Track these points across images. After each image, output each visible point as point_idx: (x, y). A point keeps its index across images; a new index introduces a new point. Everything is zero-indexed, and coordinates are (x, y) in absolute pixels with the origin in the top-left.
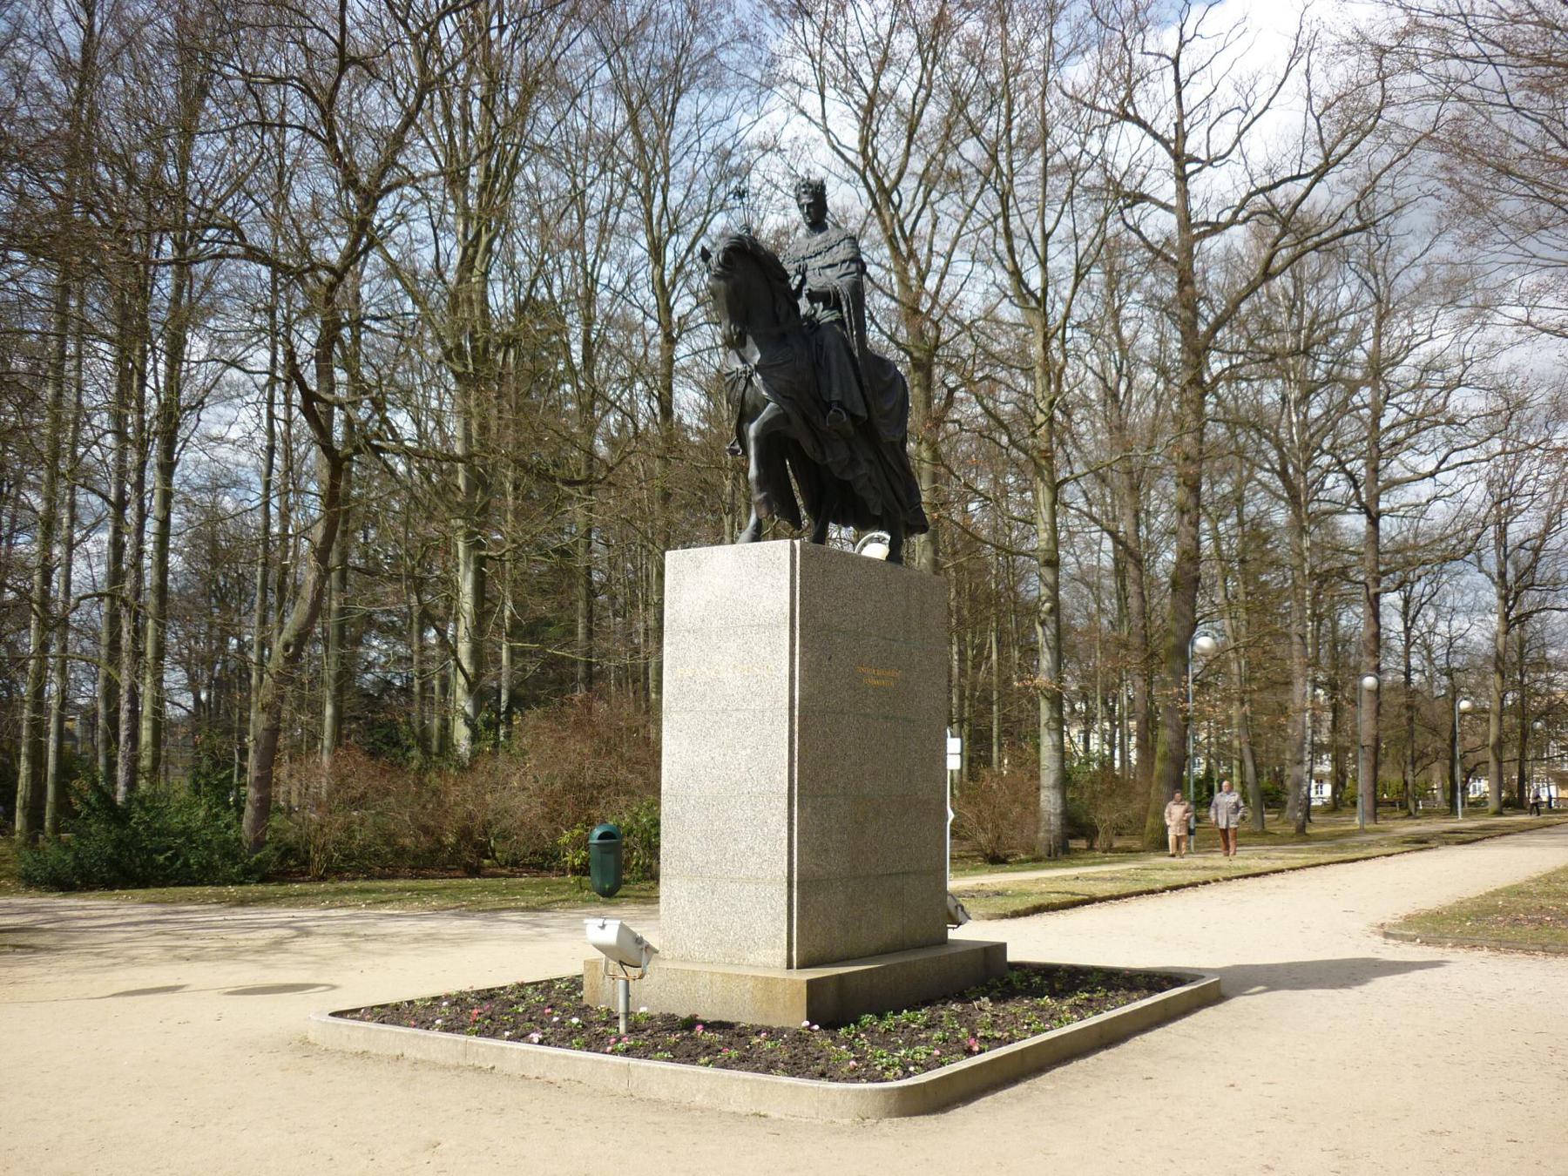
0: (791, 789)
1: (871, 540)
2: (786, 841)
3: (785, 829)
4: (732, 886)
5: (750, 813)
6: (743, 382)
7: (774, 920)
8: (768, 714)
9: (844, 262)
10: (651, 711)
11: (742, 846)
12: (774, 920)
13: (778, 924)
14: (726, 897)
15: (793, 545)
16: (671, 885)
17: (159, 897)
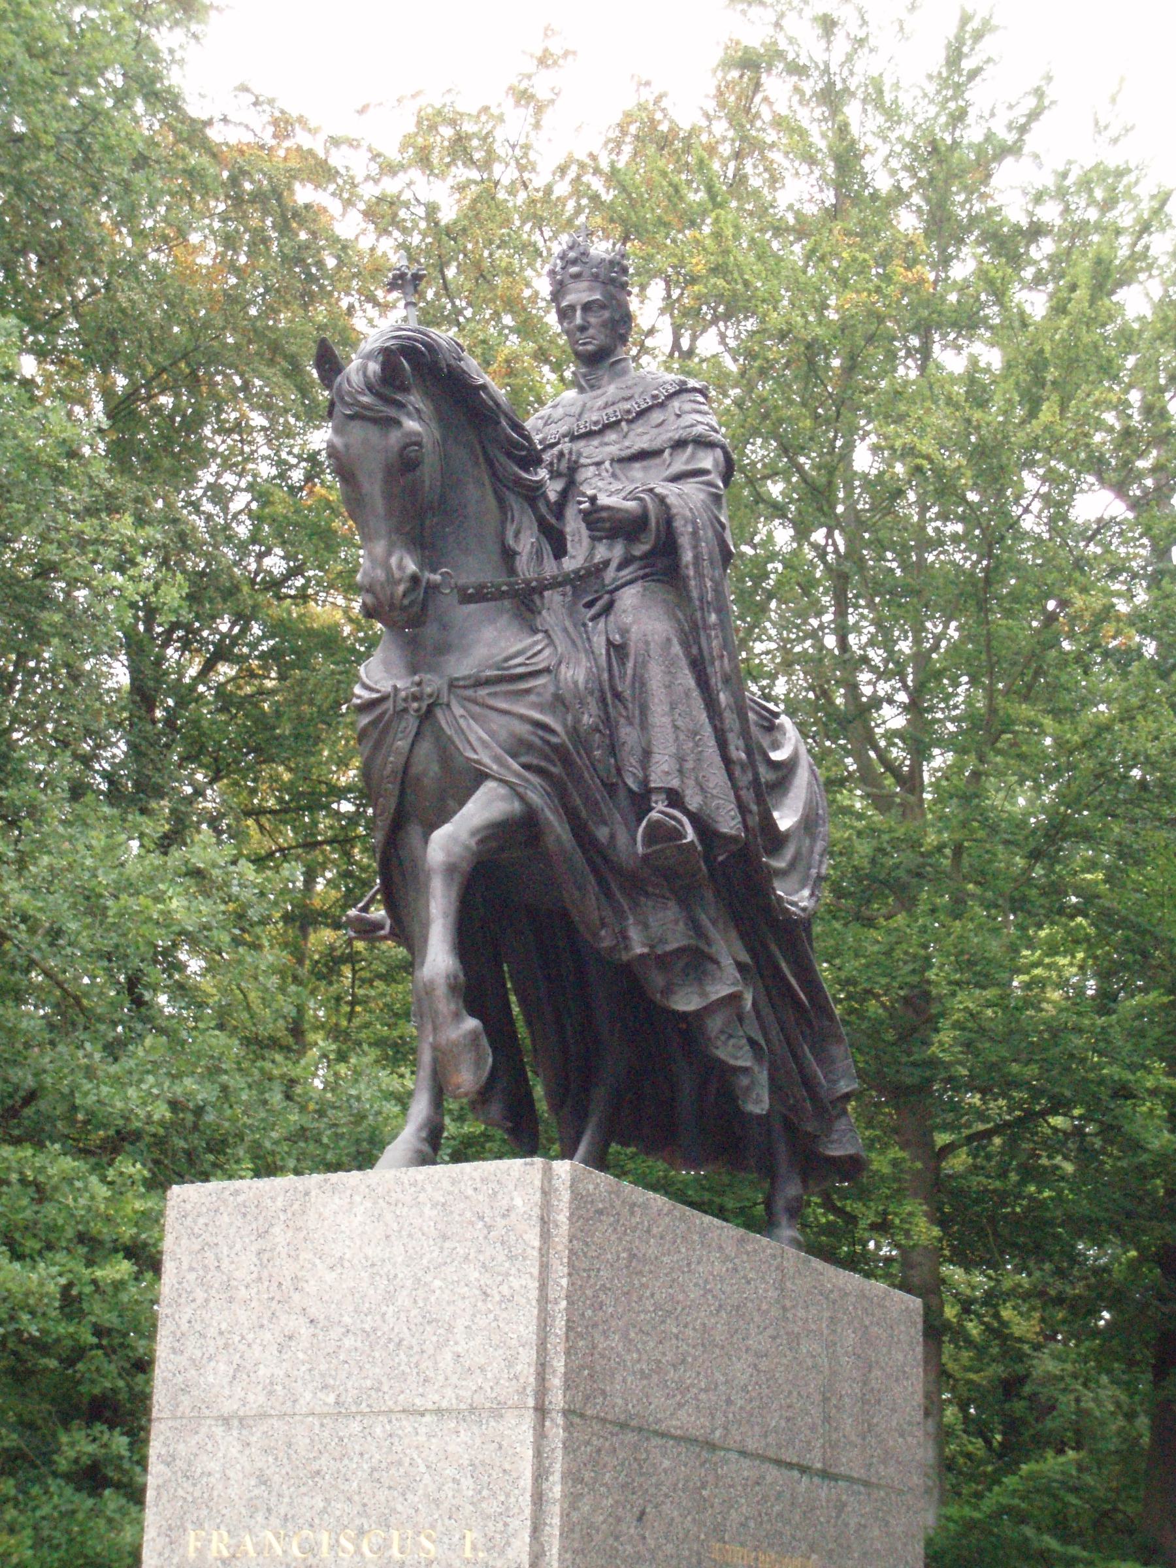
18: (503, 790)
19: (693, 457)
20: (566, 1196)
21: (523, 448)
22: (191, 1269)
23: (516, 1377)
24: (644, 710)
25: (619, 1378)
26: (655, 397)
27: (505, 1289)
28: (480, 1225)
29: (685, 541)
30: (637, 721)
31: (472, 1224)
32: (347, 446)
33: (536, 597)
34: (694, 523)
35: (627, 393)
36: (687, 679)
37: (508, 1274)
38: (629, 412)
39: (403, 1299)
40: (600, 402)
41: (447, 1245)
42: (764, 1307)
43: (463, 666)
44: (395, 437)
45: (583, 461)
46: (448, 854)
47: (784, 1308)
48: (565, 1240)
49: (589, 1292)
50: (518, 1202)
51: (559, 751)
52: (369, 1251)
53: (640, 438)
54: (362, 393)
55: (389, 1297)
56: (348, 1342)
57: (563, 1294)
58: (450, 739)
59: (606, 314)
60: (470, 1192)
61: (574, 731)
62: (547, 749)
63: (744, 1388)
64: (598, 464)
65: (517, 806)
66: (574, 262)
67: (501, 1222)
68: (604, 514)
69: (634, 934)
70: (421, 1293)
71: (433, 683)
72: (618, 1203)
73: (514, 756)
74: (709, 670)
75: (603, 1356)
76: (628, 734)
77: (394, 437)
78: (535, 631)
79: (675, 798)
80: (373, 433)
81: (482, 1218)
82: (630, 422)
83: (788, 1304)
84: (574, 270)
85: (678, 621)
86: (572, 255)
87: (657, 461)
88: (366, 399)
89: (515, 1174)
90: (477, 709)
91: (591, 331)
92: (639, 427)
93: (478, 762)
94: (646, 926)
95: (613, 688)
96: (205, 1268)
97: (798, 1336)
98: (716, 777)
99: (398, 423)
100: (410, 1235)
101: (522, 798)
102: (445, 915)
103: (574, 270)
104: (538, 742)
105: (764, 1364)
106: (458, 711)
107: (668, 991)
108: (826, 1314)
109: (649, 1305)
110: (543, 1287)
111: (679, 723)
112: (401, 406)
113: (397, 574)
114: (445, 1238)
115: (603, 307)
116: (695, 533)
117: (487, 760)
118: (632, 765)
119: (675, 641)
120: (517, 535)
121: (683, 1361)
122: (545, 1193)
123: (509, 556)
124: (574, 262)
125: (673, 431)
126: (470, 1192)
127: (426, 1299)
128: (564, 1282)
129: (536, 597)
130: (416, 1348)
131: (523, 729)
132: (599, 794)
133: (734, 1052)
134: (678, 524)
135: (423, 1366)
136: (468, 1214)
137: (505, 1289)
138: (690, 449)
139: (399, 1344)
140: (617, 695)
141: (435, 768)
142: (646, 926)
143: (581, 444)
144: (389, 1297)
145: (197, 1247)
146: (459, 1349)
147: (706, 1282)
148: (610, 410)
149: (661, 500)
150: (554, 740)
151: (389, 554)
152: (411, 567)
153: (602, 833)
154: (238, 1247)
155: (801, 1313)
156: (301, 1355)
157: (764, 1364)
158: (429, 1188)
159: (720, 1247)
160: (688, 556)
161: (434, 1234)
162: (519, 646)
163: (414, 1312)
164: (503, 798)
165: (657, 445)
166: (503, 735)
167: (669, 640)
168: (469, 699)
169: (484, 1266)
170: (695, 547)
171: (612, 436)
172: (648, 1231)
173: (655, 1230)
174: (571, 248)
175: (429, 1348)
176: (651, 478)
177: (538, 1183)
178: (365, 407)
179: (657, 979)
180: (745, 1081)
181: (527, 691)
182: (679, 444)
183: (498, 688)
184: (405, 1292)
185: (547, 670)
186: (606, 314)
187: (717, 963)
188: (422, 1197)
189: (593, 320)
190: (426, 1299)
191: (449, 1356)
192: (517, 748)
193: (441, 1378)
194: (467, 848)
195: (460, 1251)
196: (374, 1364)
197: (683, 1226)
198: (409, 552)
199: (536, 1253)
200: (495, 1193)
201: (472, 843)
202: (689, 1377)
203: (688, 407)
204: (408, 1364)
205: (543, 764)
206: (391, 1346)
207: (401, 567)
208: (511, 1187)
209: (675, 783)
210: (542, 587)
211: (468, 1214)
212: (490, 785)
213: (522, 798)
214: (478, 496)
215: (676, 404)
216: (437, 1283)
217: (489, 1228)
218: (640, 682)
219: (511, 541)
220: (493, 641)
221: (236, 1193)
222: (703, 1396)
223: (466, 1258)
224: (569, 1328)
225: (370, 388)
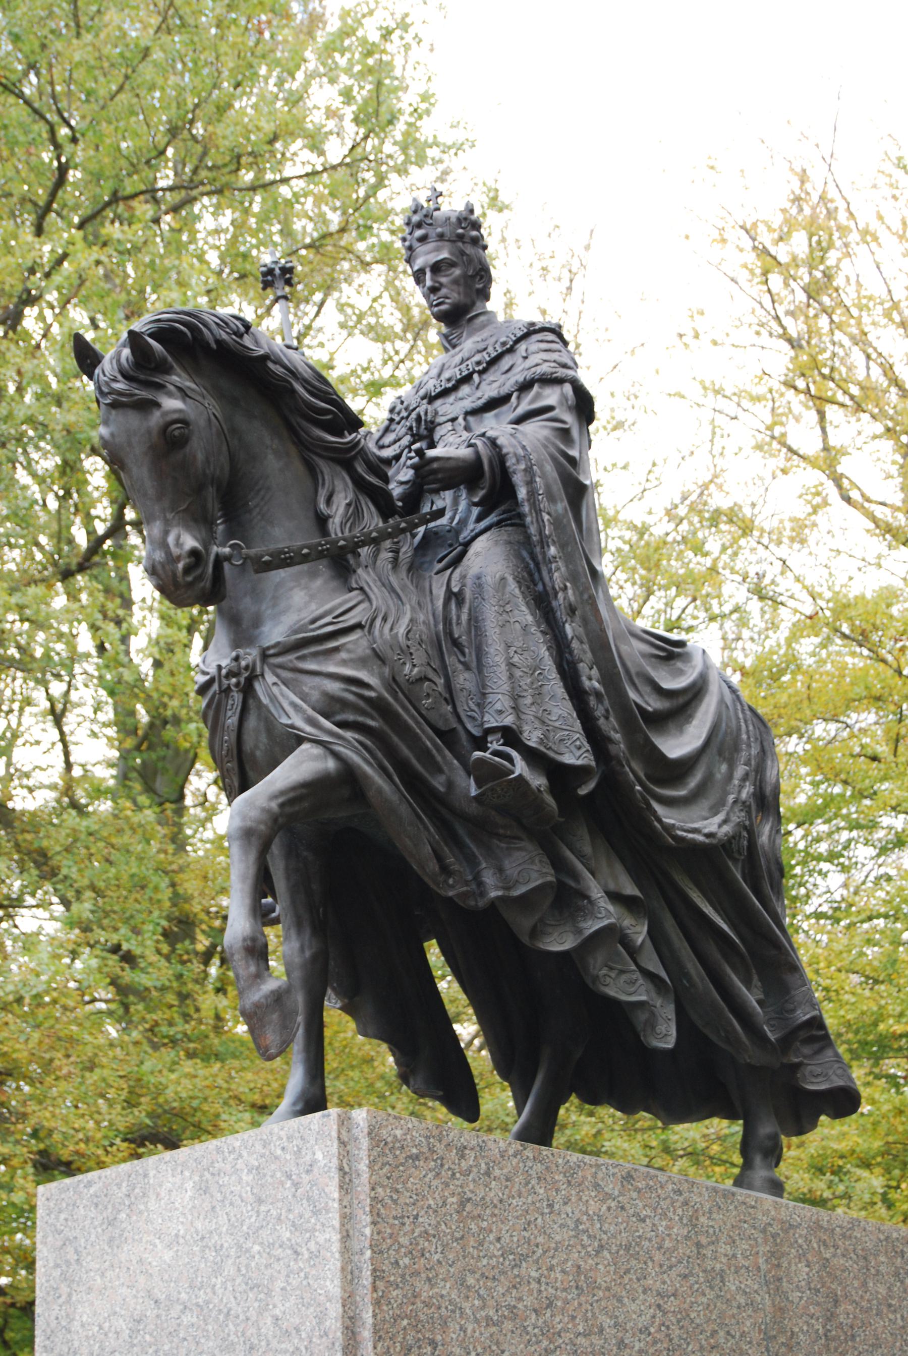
6: (237, 697)
18: (317, 750)
19: (538, 397)
20: (365, 1143)
21: (328, 412)
22: (57, 1266)
23: (326, 1334)
24: (480, 653)
25: (453, 1326)
26: (504, 344)
27: (312, 1246)
28: (288, 1184)
29: (518, 479)
30: (474, 665)
31: (282, 1183)
32: (112, 435)
33: (350, 557)
34: (527, 457)
35: (481, 346)
36: (525, 615)
37: (315, 1230)
38: (478, 363)
39: (229, 1268)
40: (458, 359)
41: (263, 1208)
42: (667, 1244)
43: (275, 633)
44: (155, 419)
45: (440, 419)
46: (244, 818)
47: (698, 1245)
48: (367, 1189)
49: (404, 1241)
50: (319, 1156)
51: (379, 706)
52: (199, 1225)
53: (490, 388)
54: (115, 380)
55: (217, 1270)
56: (187, 1319)
57: (367, 1245)
58: (266, 707)
59: (457, 272)
60: (279, 1152)
61: (393, 683)
62: (361, 703)
63: (645, 1330)
64: (453, 420)
65: (331, 764)
66: (419, 225)
67: (306, 1178)
68: (435, 465)
69: (489, 878)
70: (243, 1260)
71: (251, 655)
72: (440, 1148)
73: (326, 716)
74: (554, 604)
75: (427, 1305)
76: (464, 680)
77: (155, 419)
78: (351, 590)
79: (511, 736)
80: (133, 419)
81: (289, 1177)
82: (481, 373)
83: (704, 1240)
84: (419, 233)
85: (523, 560)
86: (416, 218)
87: (505, 408)
88: (120, 386)
89: (315, 1127)
90: (286, 674)
91: (444, 291)
92: (489, 377)
93: (292, 726)
94: (500, 870)
95: (449, 633)
96: (68, 1263)
97: (722, 1274)
98: (561, 709)
99: (158, 405)
100: (231, 1204)
101: (336, 755)
102: (243, 878)
103: (419, 233)
104: (351, 697)
105: (671, 1304)
106: (270, 678)
107: (535, 933)
108: (763, 1249)
109: (495, 1249)
110: (346, 1237)
111: (516, 659)
112: (160, 387)
113: (175, 551)
114: (260, 1201)
115: (452, 264)
116: (529, 470)
117: (299, 722)
118: (466, 705)
119: (510, 579)
120: (329, 501)
121: (550, 1305)
122: (342, 1143)
123: (322, 521)
124: (419, 225)
125: (518, 376)
126: (279, 1152)
127: (247, 1266)
128: (368, 1231)
129: (350, 557)
130: (242, 1317)
131: (334, 687)
132: (429, 740)
133: (626, 987)
134: (510, 462)
135: (248, 1334)
136: (278, 1175)
137: (312, 1246)
138: (536, 388)
139: (228, 1314)
140: (455, 640)
141: (264, 738)
142: (500, 870)
143: (438, 402)
144: (217, 1270)
145: (59, 1243)
146: (277, 1312)
147: (578, 1222)
148: (463, 366)
149: (493, 442)
150: (373, 694)
151: (166, 533)
152: (190, 542)
153: (438, 783)
154: (93, 1238)
155: (724, 1248)
156: (148, 1337)
157: (671, 1304)
158: (245, 1154)
159: (596, 1186)
160: (522, 493)
161: (251, 1199)
162: (328, 607)
163: (239, 1280)
164: (316, 758)
165: (505, 390)
166: (315, 696)
167: (503, 579)
168: (281, 666)
169: (294, 1225)
170: (530, 483)
171: (465, 390)
172: (488, 1173)
173: (497, 1172)
174: (415, 212)
175: (252, 1314)
176: (496, 426)
177: (334, 1134)
178: (120, 393)
179: (522, 924)
180: (642, 1016)
181: (336, 649)
182: (525, 387)
183: (305, 651)
184: (230, 1262)
185: (359, 626)
186: (457, 272)
187: (588, 898)
188: (240, 1164)
189: (444, 280)
190: (247, 1266)
191: (269, 1321)
192: (330, 707)
193: (263, 1343)
194: (268, 811)
195: (274, 1213)
196: (208, 1338)
197: (539, 1167)
198: (188, 528)
199: (336, 1205)
200: (299, 1150)
201: (274, 805)
202: (559, 1322)
203: (534, 347)
204: (236, 1334)
205: (360, 719)
206: (221, 1317)
207: (178, 544)
208: (313, 1142)
209: (508, 720)
210: (353, 547)
211: (278, 1175)
212: (305, 746)
213: (336, 755)
214: (276, 465)
215: (522, 347)
216: (257, 1248)
217: (296, 1185)
218: (475, 622)
219: (322, 506)
220: (298, 603)
221: (89, 1184)
222: (581, 1340)
223: (279, 1219)
224: (375, 1278)
225: (126, 376)
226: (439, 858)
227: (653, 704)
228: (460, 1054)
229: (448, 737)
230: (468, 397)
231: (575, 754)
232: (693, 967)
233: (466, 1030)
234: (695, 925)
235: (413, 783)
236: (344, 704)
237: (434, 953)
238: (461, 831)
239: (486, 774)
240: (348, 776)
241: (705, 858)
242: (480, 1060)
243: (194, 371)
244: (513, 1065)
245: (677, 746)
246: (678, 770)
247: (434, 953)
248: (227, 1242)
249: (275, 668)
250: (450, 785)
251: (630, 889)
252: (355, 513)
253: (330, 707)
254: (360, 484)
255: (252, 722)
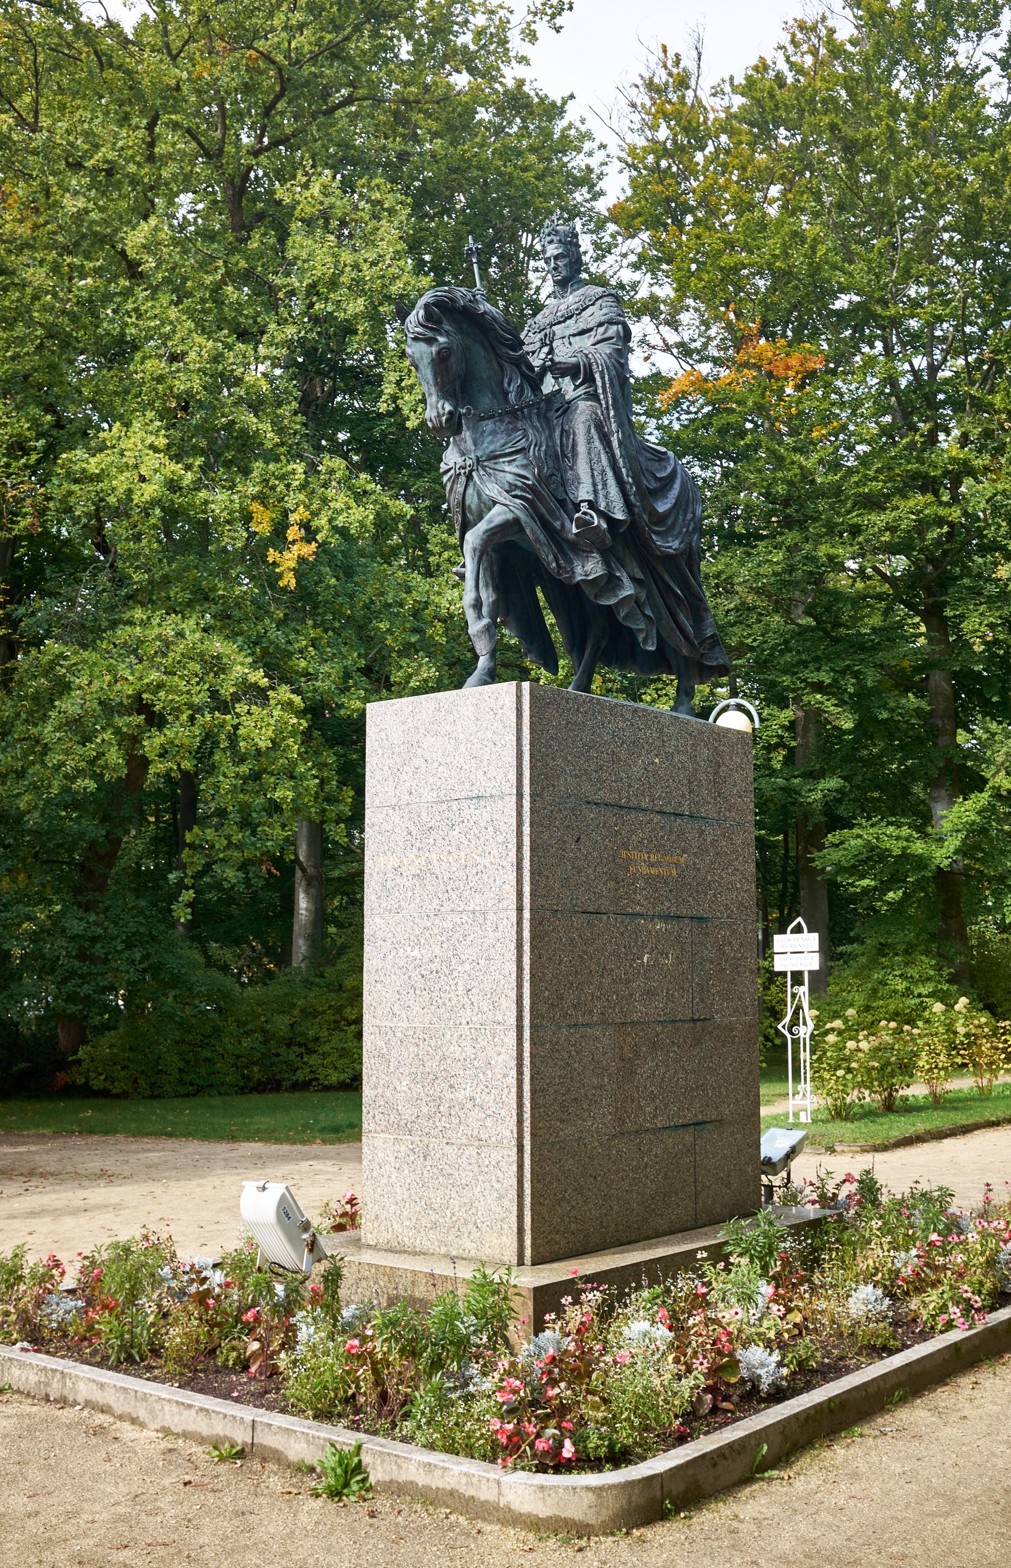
0: (520, 1018)
1: (740, 708)
2: (514, 1090)
3: (514, 1073)
4: (448, 1149)
5: (470, 1051)
6: (463, 479)
7: (500, 1198)
8: (491, 916)
9: (601, 325)
10: (357, 903)
11: (461, 1095)
12: (500, 1198)
13: (506, 1203)
14: (432, 1159)
15: (519, 688)
16: (377, 1139)
17: (896, 1134)
88: (419, 330)
132: (553, 505)
153: (557, 524)
176: (586, 343)
179: (588, 591)
192: (511, 488)
214: (483, 365)
226: (557, 561)
227: (654, 485)
228: (547, 634)
229: (562, 503)
230: (573, 325)
231: (620, 516)
232: (664, 611)
233: (550, 619)
234: (666, 591)
235: (546, 526)
236: (517, 487)
237: (538, 589)
238: (565, 546)
239: (581, 523)
240: (516, 521)
241: (669, 560)
242: (557, 637)
243: (452, 321)
244: (576, 646)
245: (662, 507)
246: (661, 519)
247: (538, 589)
248: (461, 736)
249: (484, 468)
250: (563, 525)
251: (640, 575)
252: (520, 391)
253: (511, 488)
254: (523, 376)
255: (470, 491)
